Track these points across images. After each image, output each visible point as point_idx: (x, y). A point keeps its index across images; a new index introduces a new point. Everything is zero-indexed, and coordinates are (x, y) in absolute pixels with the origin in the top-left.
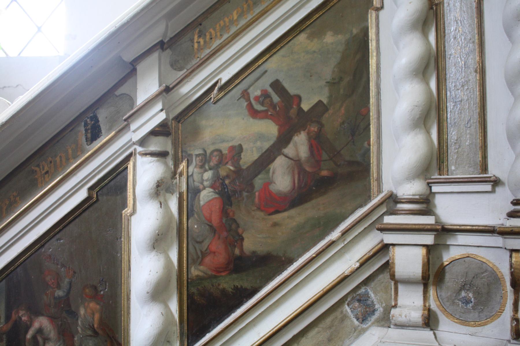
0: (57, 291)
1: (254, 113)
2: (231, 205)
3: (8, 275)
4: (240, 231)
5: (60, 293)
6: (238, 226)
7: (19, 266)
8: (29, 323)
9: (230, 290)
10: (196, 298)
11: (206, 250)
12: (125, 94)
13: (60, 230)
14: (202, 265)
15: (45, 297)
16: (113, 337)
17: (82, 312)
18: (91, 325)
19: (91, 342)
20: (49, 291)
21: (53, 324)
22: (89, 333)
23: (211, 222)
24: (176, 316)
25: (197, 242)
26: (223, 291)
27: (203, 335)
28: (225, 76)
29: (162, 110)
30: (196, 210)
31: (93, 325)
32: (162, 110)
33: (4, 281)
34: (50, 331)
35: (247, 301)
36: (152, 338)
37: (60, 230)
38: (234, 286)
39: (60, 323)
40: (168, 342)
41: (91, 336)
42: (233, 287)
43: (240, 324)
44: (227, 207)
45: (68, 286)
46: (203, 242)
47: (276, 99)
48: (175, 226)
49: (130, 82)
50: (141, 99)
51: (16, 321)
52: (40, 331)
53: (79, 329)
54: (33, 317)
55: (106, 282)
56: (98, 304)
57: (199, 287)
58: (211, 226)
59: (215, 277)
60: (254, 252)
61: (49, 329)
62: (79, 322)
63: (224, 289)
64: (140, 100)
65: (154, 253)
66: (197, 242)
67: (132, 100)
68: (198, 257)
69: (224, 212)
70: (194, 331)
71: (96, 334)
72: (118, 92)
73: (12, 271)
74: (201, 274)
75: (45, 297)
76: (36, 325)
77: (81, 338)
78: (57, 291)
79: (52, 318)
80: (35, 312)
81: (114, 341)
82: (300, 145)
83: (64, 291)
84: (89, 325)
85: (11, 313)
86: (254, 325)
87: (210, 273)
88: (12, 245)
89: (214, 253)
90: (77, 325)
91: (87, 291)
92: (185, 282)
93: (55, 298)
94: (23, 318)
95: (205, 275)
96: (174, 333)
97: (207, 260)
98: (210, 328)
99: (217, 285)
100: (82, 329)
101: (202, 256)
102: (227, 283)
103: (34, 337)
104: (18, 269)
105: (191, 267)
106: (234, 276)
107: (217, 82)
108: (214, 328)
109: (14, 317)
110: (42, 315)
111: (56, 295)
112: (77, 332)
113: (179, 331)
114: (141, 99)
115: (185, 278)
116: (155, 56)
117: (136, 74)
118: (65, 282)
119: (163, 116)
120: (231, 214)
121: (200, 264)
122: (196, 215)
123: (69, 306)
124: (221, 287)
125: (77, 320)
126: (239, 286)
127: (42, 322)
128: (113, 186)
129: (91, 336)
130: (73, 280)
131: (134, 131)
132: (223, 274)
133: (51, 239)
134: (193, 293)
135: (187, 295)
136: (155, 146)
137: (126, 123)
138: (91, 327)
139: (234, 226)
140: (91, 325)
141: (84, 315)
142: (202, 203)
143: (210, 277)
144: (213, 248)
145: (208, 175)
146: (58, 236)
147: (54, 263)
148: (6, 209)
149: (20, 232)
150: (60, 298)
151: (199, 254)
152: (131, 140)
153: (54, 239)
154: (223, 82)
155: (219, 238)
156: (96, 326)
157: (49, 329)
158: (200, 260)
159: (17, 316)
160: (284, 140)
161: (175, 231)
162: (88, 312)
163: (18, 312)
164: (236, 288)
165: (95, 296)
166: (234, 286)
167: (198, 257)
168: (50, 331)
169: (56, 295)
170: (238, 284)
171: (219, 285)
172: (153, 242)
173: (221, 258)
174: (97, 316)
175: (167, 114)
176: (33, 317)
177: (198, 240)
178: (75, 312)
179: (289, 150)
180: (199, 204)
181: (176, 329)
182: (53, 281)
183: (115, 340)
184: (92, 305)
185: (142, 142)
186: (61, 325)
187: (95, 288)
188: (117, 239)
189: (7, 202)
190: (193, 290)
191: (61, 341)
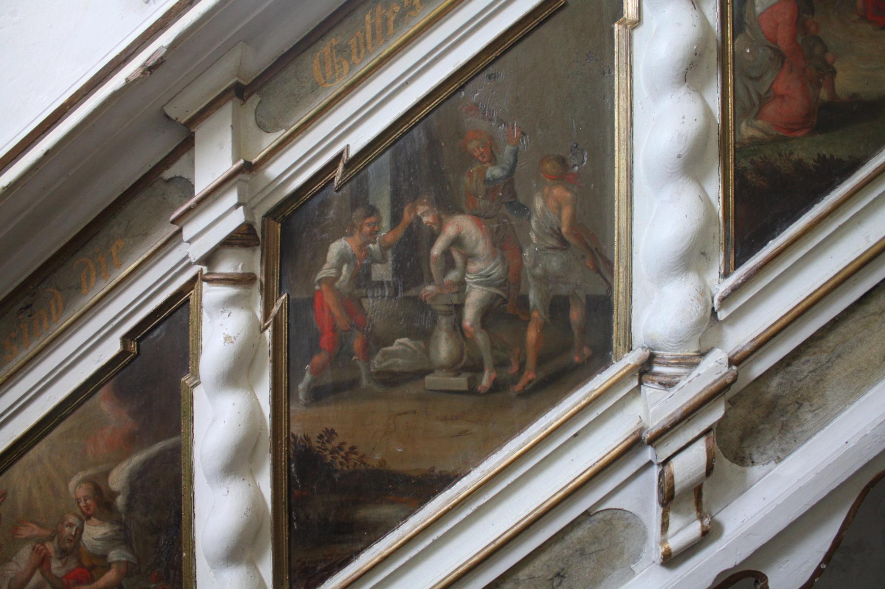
0: (490, 168)
2: (812, 12)
3: (396, 141)
4: (829, 57)
5: (495, 172)
6: (825, 50)
7: (417, 124)
8: (435, 228)
9: (811, 162)
10: (749, 177)
11: (768, 91)
12: (175, 177)
13: (497, 58)
14: (761, 119)
15: (467, 180)
16: (596, 249)
17: (538, 204)
18: (556, 228)
19: (554, 259)
20: (475, 169)
21: (482, 229)
22: (552, 242)
23: (775, 43)
24: (719, 207)
25: (751, 78)
26: (800, 162)
27: (763, 243)
28: (357, 142)
29: (237, 206)
30: (748, 22)
31: (560, 231)
32: (237, 206)
33: (388, 153)
34: (477, 242)
35: (841, 182)
36: (688, 239)
37: (497, 58)
38: (819, 155)
39: (495, 226)
40: (703, 254)
41: (555, 248)
42: (816, 158)
43: (842, 215)
44: (805, 16)
45: (511, 159)
46: (761, 77)
48: (713, 47)
49: (185, 158)
50: (202, 184)
51: (411, 225)
52: (457, 241)
53: (533, 236)
54: (443, 216)
55: (582, 151)
56: (568, 189)
57: (755, 158)
58: (777, 51)
59: (785, 140)
60: (855, 95)
61: (474, 238)
62: (533, 224)
63: (801, 160)
64: (201, 186)
65: (684, 89)
66: (751, 78)
67: (188, 187)
68: (753, 105)
69: (799, 24)
70: (746, 238)
71: (564, 244)
72: (168, 174)
73: (404, 134)
74: (758, 134)
75: (467, 180)
76: (450, 231)
77: (537, 252)
78: (490, 168)
79: (479, 217)
80: (448, 205)
81: (598, 257)
83: (503, 168)
84: (552, 228)
85: (402, 210)
86: (859, 223)
87: (774, 132)
88: (407, 84)
89: (782, 96)
90: (529, 228)
91: (548, 166)
92: (731, 147)
93: (486, 181)
94: (425, 219)
95: (766, 136)
96: (714, 238)
97: (770, 109)
98: (774, 230)
99: (787, 153)
100: (537, 236)
101: (760, 103)
102: (806, 150)
103: (446, 253)
104: (415, 131)
105: (741, 122)
106: (820, 137)
107: (339, 157)
108: (783, 230)
109: (407, 217)
110: (462, 212)
111: (488, 175)
112: (529, 241)
113: (722, 234)
114: (202, 184)
115: (731, 140)
116: (226, 113)
117: (193, 145)
118: (506, 151)
119: (238, 218)
120: (813, 28)
121: (757, 117)
122: (748, 31)
123: (514, 195)
124: (794, 157)
125: (529, 219)
126: (828, 156)
127: (461, 225)
128: (174, 318)
129: (555, 248)
130: (521, 148)
131: (189, 242)
132: (799, 134)
133: (477, 74)
134: (745, 169)
135: (735, 170)
136: (227, 267)
137: (176, 228)
138: (555, 232)
139: (817, 50)
140: (556, 228)
141: (542, 210)
142: (759, 9)
143: (776, 140)
144: (781, 89)
146: (491, 70)
147: (483, 118)
148: (396, 22)
149: (425, 58)
150: (495, 180)
151: (754, 96)
152: (187, 257)
153: (484, 75)
154: (352, 152)
155: (791, 71)
156: (564, 230)
157: (474, 238)
158: (756, 109)
159: (412, 215)
161: (714, 56)
162: (549, 205)
163: (414, 209)
164: (822, 159)
165: (563, 173)
166: (819, 155)
167: (753, 105)
168: (477, 242)
169: (488, 175)
170: (825, 152)
171: (791, 153)
172: (683, 69)
173: (796, 105)
174: (566, 213)
175: (249, 212)
176: (443, 216)
177: (753, 74)
178: (524, 206)
180: (754, 11)
181: (718, 231)
182: (482, 150)
183: (600, 255)
184: (557, 192)
185: (209, 259)
186: (498, 229)
187: (563, 161)
188: (604, 74)
189: (397, 9)
190: (745, 163)
191: (498, 260)
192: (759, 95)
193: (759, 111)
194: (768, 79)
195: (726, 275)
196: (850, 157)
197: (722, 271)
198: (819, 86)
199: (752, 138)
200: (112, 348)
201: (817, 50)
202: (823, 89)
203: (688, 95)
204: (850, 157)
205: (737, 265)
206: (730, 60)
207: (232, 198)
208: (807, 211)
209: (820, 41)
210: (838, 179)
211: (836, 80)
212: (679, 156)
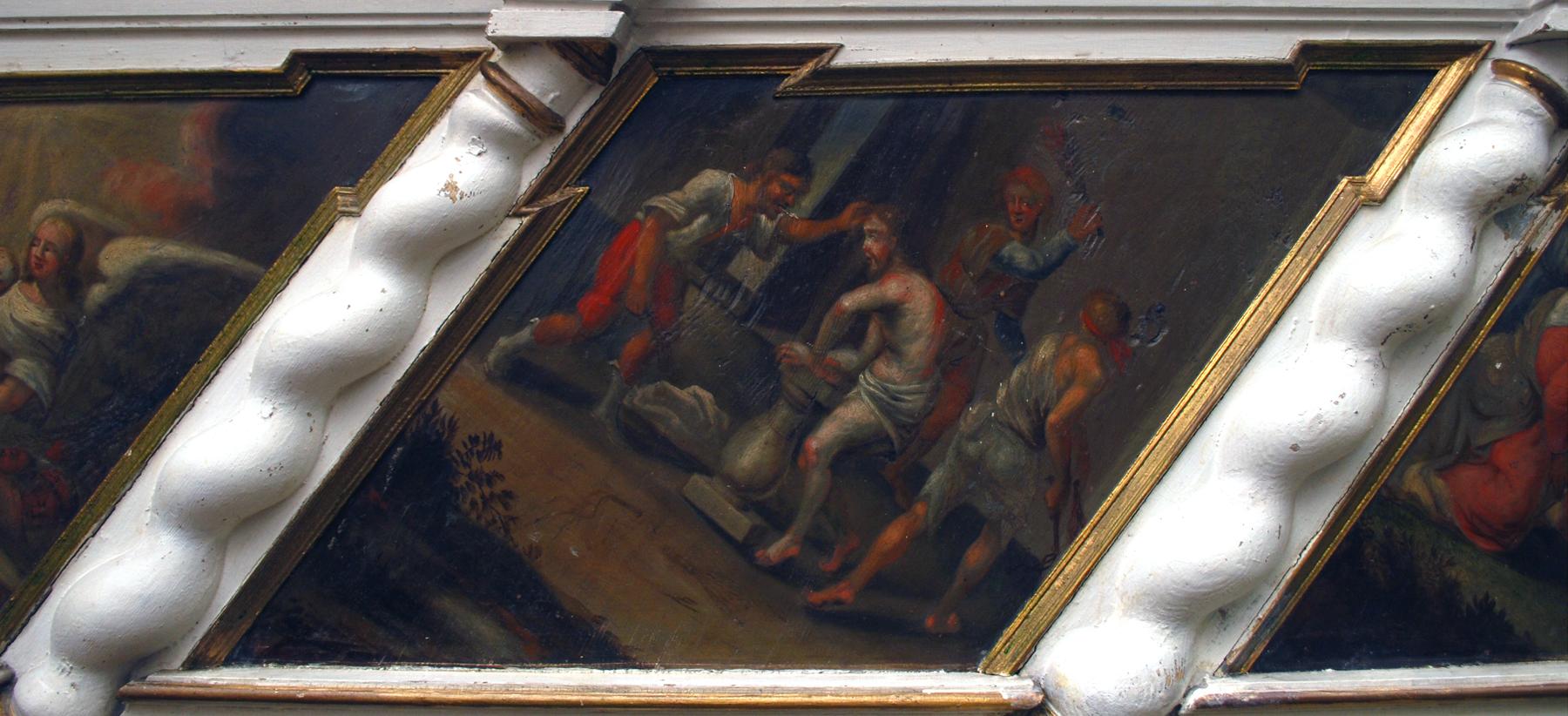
9: (1469, 599)
10: (1369, 550)
11: (1480, 448)
25: (1475, 410)
42: (1480, 597)
46: (1488, 418)
57: (1396, 530)
58: (1537, 398)
65: (1367, 355)
66: (1475, 410)
74: (1425, 497)
97: (1468, 475)
121: (1442, 472)
122: (1517, 336)
124: (1452, 573)
126: (1498, 608)
132: (1481, 544)
142: (1555, 318)
164: (1486, 606)
166: (1487, 596)
170: (1499, 599)
171: (1451, 563)
177: (1481, 405)
180: (1547, 315)
185: (516, 47)
194: (1498, 429)
196: (1527, 633)
197: (1231, 661)
199: (1413, 497)
202: (1558, 506)
204: (1527, 633)
205: (1263, 665)
212: (1295, 448)
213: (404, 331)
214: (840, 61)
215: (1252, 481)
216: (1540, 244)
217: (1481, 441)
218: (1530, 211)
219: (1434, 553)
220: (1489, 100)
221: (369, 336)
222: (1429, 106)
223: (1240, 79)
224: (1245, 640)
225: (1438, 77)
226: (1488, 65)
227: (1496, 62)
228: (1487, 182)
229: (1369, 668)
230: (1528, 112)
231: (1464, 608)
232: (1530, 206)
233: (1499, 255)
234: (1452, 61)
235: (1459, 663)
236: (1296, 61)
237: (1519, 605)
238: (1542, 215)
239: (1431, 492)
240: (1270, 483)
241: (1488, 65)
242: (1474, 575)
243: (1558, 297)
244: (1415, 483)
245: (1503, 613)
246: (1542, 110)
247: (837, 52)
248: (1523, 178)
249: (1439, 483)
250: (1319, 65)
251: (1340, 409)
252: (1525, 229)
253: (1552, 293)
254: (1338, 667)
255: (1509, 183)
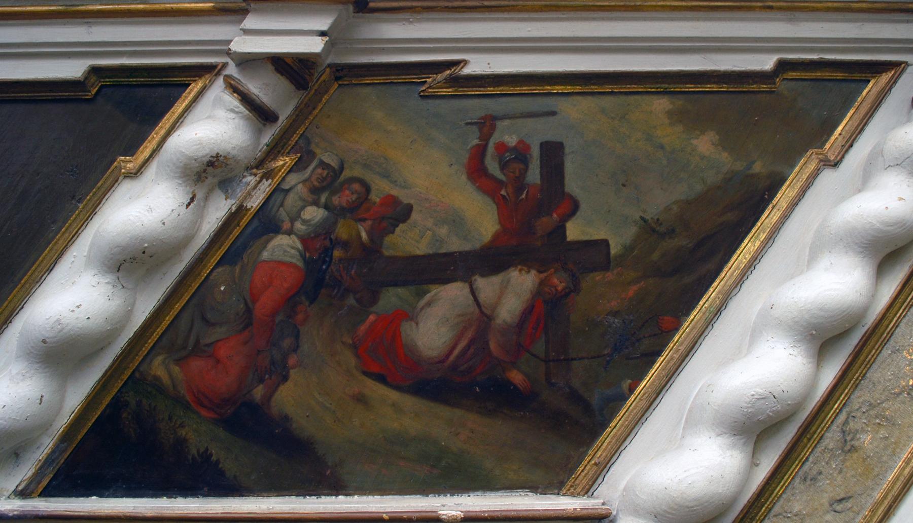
1: (476, 171)
2: (312, 300)
4: (292, 360)
6: (295, 349)
9: (194, 451)
10: (125, 415)
11: (208, 345)
23: (255, 299)
25: (204, 319)
29: (323, 34)
32: (323, 34)
38: (207, 449)
42: (202, 450)
44: (303, 298)
46: (214, 325)
47: (534, 175)
57: (144, 401)
58: (249, 311)
59: (187, 407)
60: (286, 418)
63: (185, 440)
65: (109, 278)
66: (204, 319)
74: (166, 379)
82: (512, 293)
87: (183, 391)
89: (218, 361)
92: (128, 373)
97: (197, 364)
105: (159, 354)
106: (221, 433)
119: (315, 45)
120: (300, 317)
121: (178, 362)
122: (238, 269)
124: (183, 432)
126: (214, 458)
132: (204, 413)
139: (287, 343)
142: (265, 255)
145: (315, 214)
155: (246, 343)
160: (492, 259)
164: (206, 456)
166: (207, 449)
170: (216, 453)
171: (182, 426)
175: (329, 47)
177: (209, 316)
179: (487, 286)
180: (260, 253)
185: (247, 61)
192: (197, 342)
193: (186, 357)
194: (219, 333)
195: (23, 493)
196: (235, 477)
197: (20, 488)
198: (261, 380)
199: (157, 378)
200: (72, 70)
201: (287, 343)
202: (261, 387)
203: (110, 287)
204: (235, 477)
205: (47, 493)
206: (195, 286)
207: (323, 23)
208: (152, 496)
209: (297, 336)
210: (206, 489)
211: (282, 388)
212: (44, 341)
213: (128, 314)
214: (467, 71)
215: (26, 363)
216: (254, 203)
217: (208, 341)
218: (244, 180)
219: (170, 418)
220: (218, 102)
221: (86, 323)
222: (179, 107)
223: (51, 91)
224: (30, 474)
225: (190, 87)
226: (220, 81)
227: (226, 76)
228: (190, 158)
229: (122, 497)
230: (232, 111)
231: (190, 457)
232: (244, 177)
233: (218, 210)
234: (200, 77)
235: (185, 496)
236: (86, 78)
237: (229, 456)
238: (253, 183)
239: (171, 376)
240: (36, 366)
241: (220, 81)
242: (199, 435)
243: (272, 238)
244: (159, 368)
245: (218, 462)
246: (242, 108)
247: (465, 64)
248: (218, 156)
249: (176, 369)
250: (108, 81)
251: (75, 315)
252: (240, 192)
253: (265, 237)
254: (101, 496)
255: (207, 159)
